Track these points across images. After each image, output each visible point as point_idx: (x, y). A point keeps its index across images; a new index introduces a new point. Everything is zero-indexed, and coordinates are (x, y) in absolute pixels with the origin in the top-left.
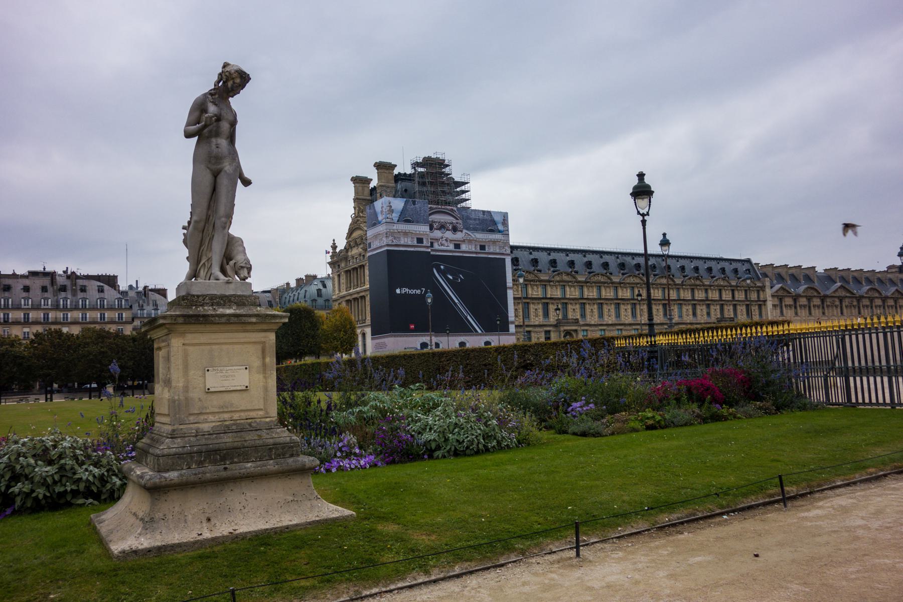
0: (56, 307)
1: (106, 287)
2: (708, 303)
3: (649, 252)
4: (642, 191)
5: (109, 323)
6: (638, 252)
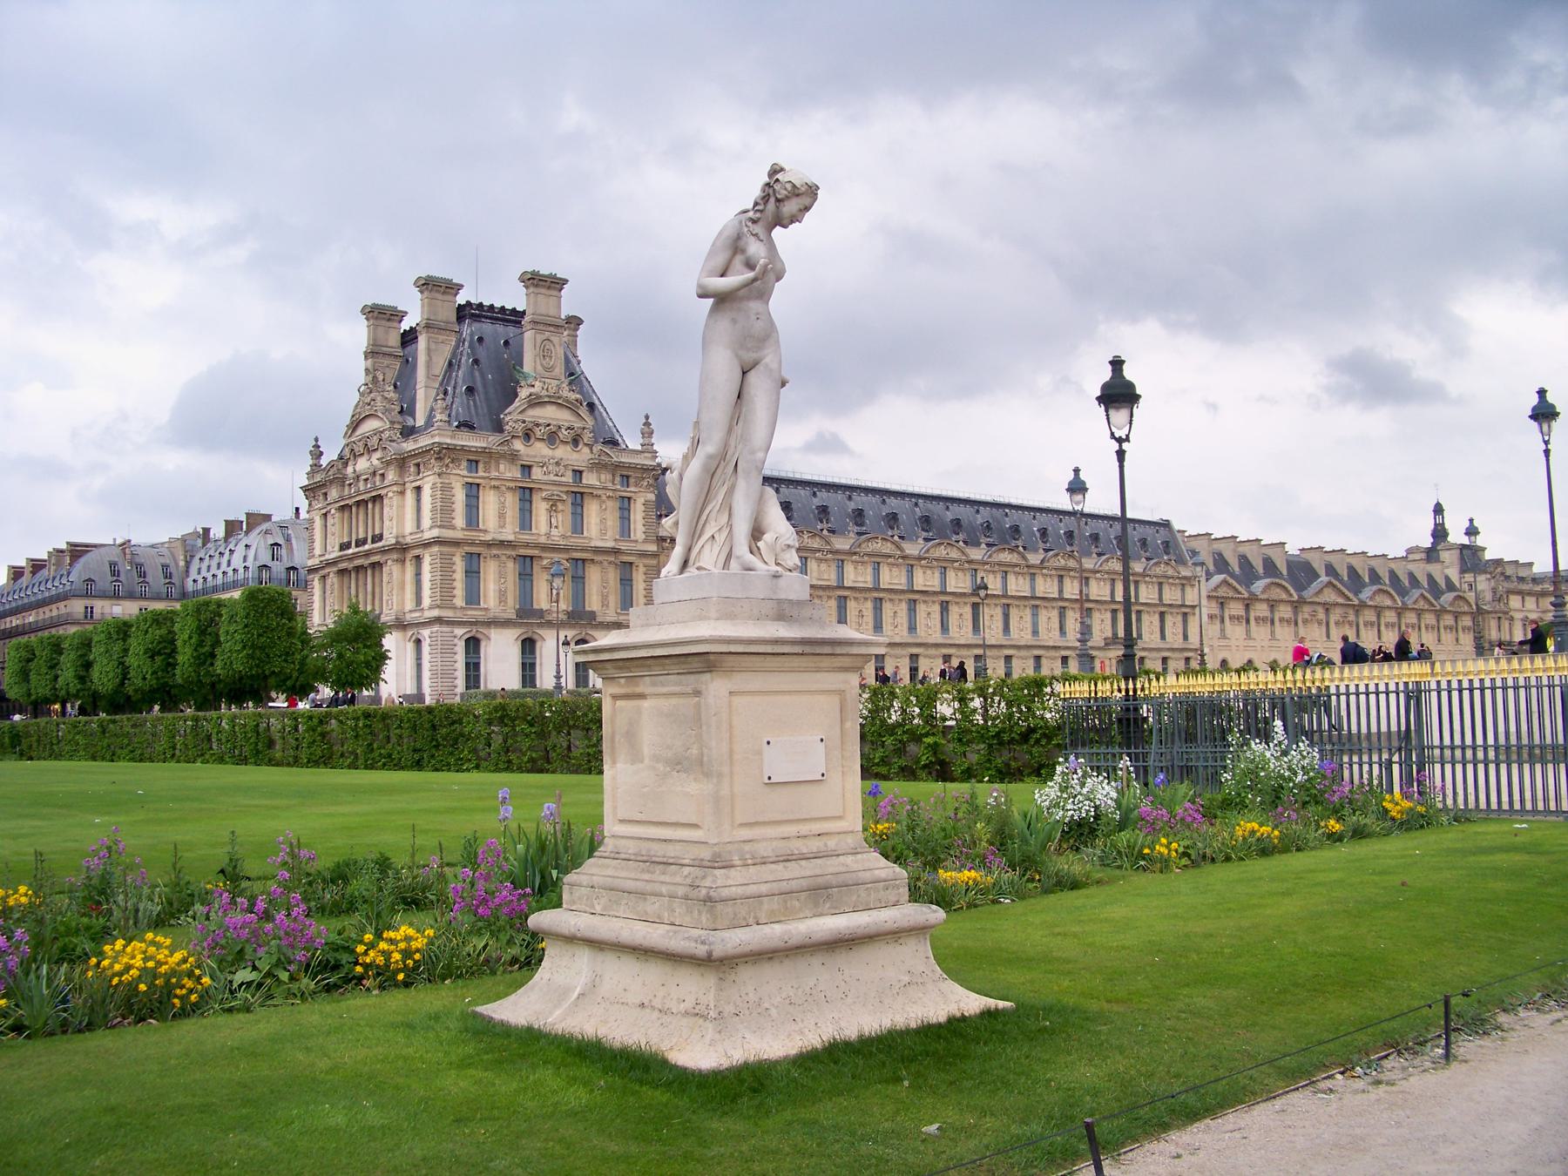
3: (1129, 515)
6: (1109, 513)
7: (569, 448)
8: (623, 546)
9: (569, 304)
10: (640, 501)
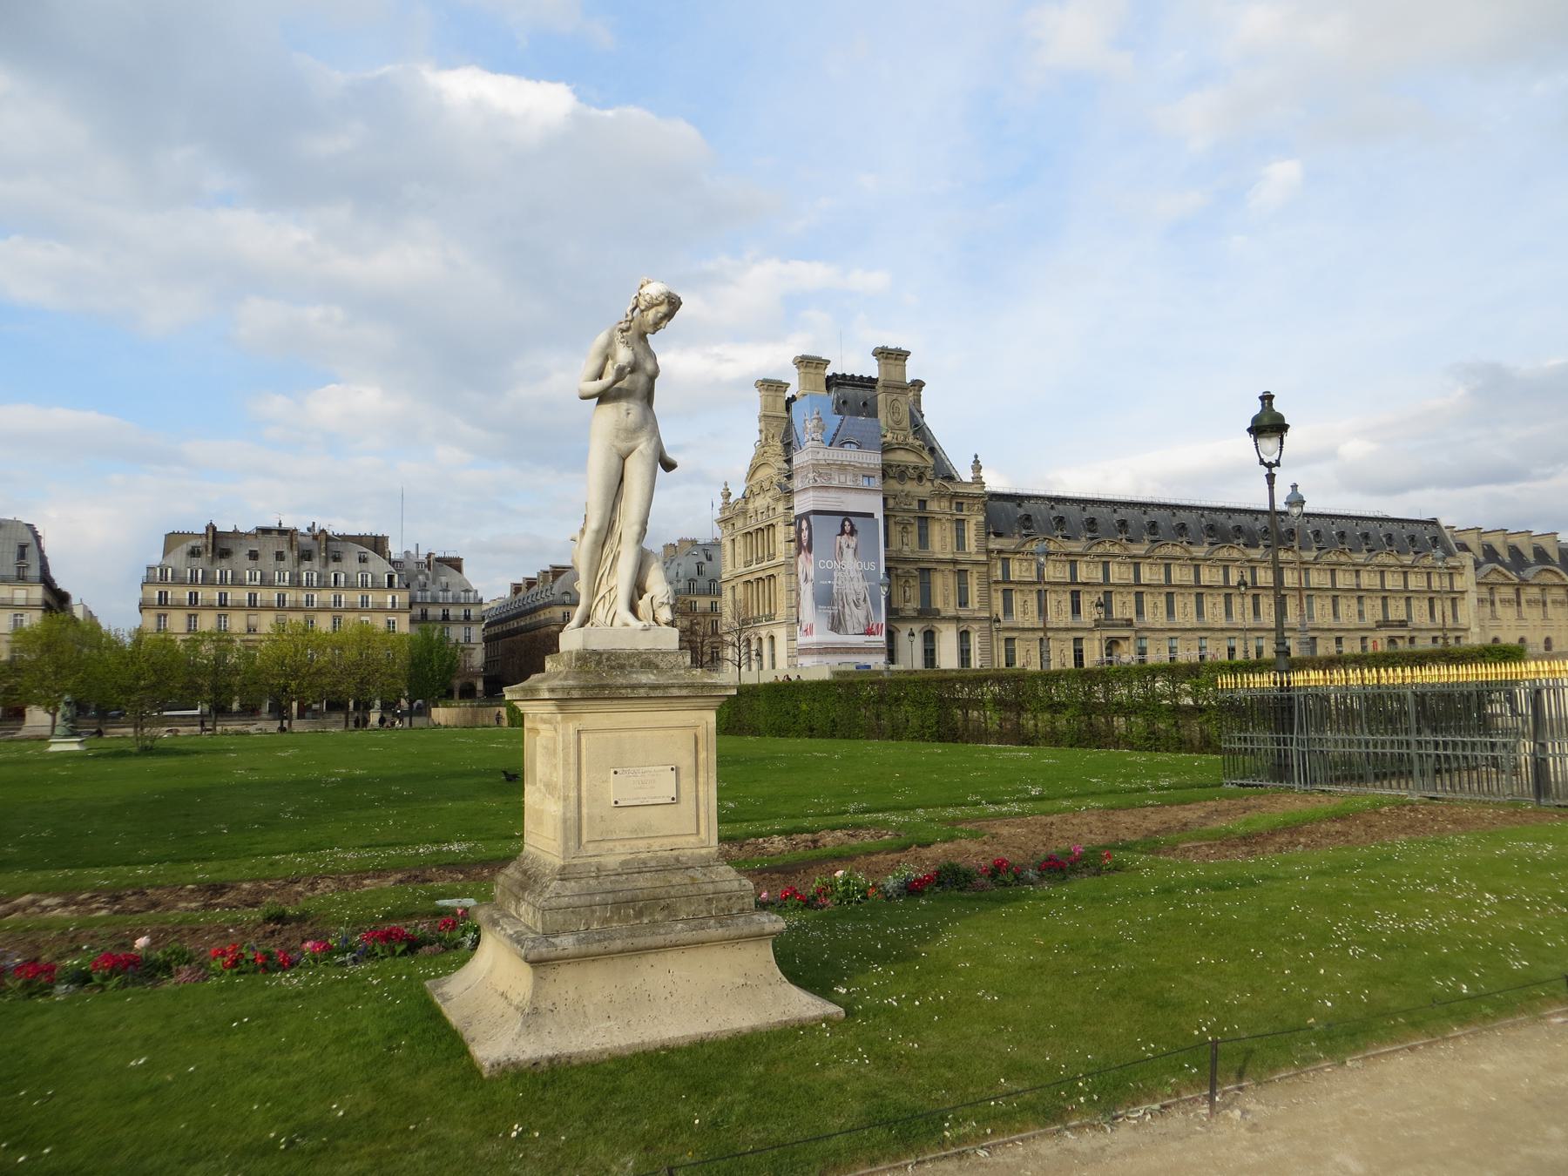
0: (296, 583)
1: (371, 554)
2: (1360, 594)
4: (1269, 425)
5: (374, 610)
7: (915, 483)
8: (960, 557)
9: (911, 372)
10: (973, 522)
